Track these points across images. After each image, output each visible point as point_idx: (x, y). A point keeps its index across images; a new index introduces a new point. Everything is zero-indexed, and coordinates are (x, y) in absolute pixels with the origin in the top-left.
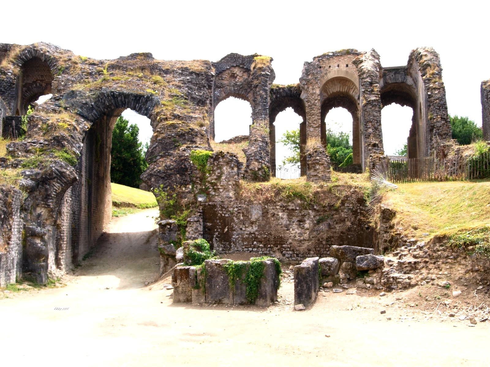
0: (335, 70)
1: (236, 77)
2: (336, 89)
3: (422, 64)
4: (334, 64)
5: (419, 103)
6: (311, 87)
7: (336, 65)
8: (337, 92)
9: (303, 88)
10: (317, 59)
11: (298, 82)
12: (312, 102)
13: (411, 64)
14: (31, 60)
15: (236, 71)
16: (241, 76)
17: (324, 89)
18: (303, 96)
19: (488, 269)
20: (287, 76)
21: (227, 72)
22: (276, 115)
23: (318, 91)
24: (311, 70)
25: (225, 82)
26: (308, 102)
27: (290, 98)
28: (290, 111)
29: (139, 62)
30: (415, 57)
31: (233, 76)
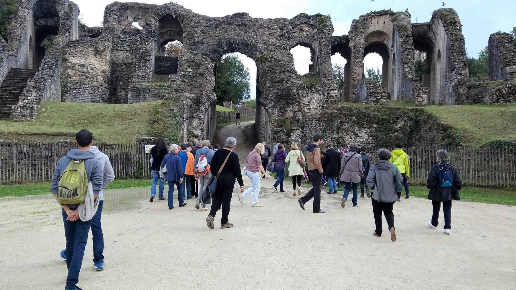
0: (376, 26)
1: (303, 31)
2: (375, 39)
3: (448, 19)
4: (375, 22)
5: (437, 52)
6: (357, 39)
7: (376, 22)
8: (375, 42)
9: (351, 39)
10: (362, 18)
11: (347, 34)
12: (358, 49)
13: (433, 22)
14: (165, 16)
15: (305, 27)
16: (313, 28)
17: (366, 40)
18: (351, 44)
19: (1, 24)
20: (341, 29)
21: (298, 27)
22: (371, 52)
23: (362, 41)
24: (358, 26)
25: (296, 34)
26: (354, 49)
27: (341, 46)
28: (338, 55)
29: (239, 21)
30: (438, 15)
31: (302, 30)
